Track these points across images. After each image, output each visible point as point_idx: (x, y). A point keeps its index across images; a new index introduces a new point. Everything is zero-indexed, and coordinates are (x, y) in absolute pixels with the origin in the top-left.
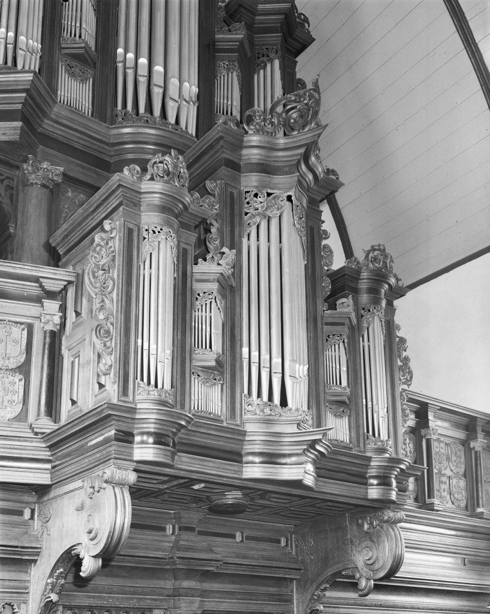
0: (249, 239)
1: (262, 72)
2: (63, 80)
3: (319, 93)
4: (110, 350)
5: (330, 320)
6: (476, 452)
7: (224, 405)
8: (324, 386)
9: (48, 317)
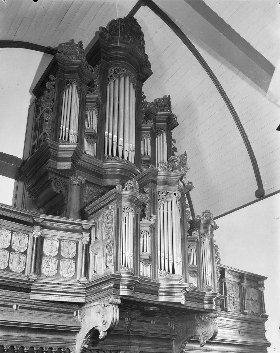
0: (160, 210)
1: (159, 137)
3: (186, 156)
4: (111, 254)
5: (190, 240)
6: (244, 288)
7: (152, 273)
9: (85, 239)
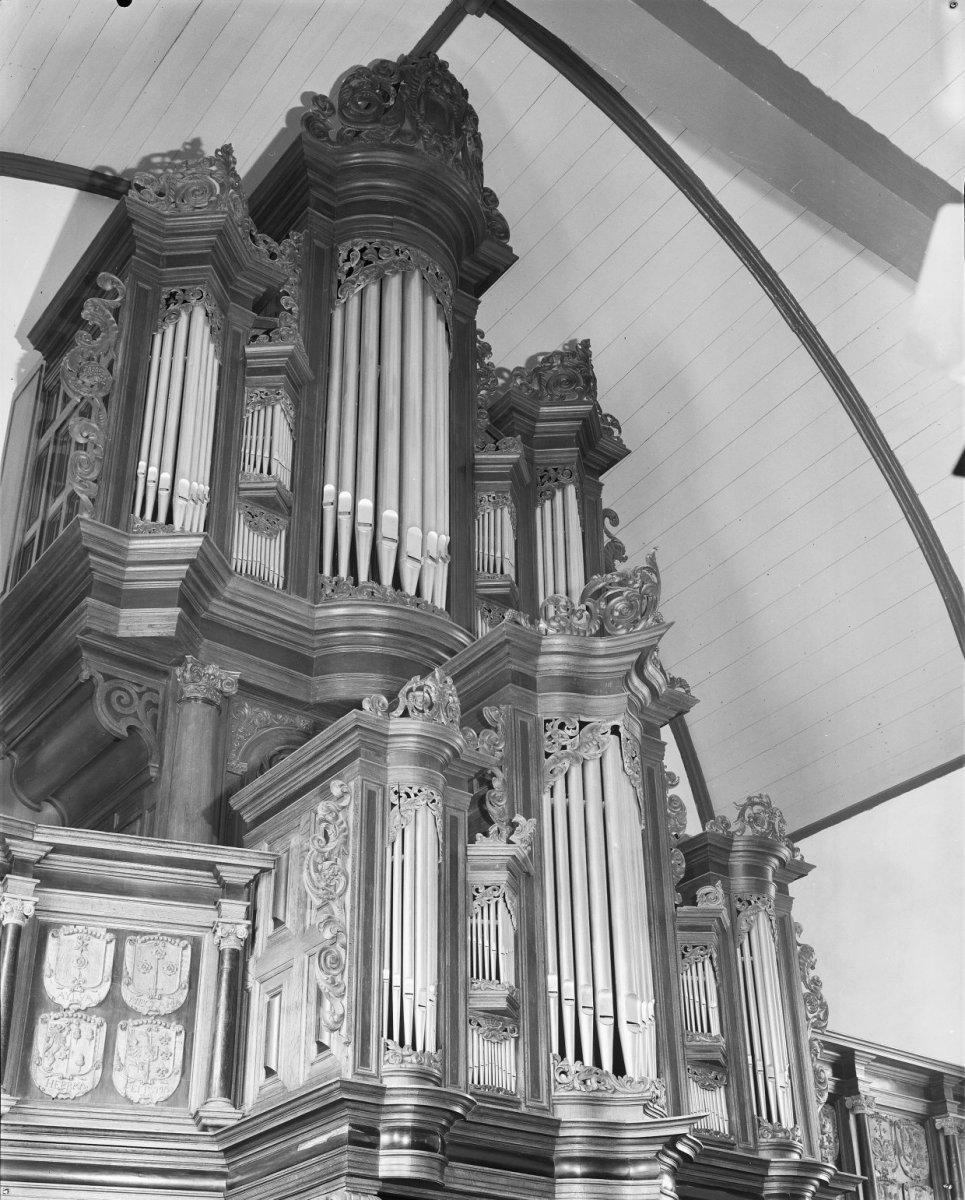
0: (552, 797)
1: (548, 504)
2: (246, 547)
3: (657, 575)
6: (947, 1138)
7: (521, 1075)
8: (683, 1035)
9: (228, 927)
